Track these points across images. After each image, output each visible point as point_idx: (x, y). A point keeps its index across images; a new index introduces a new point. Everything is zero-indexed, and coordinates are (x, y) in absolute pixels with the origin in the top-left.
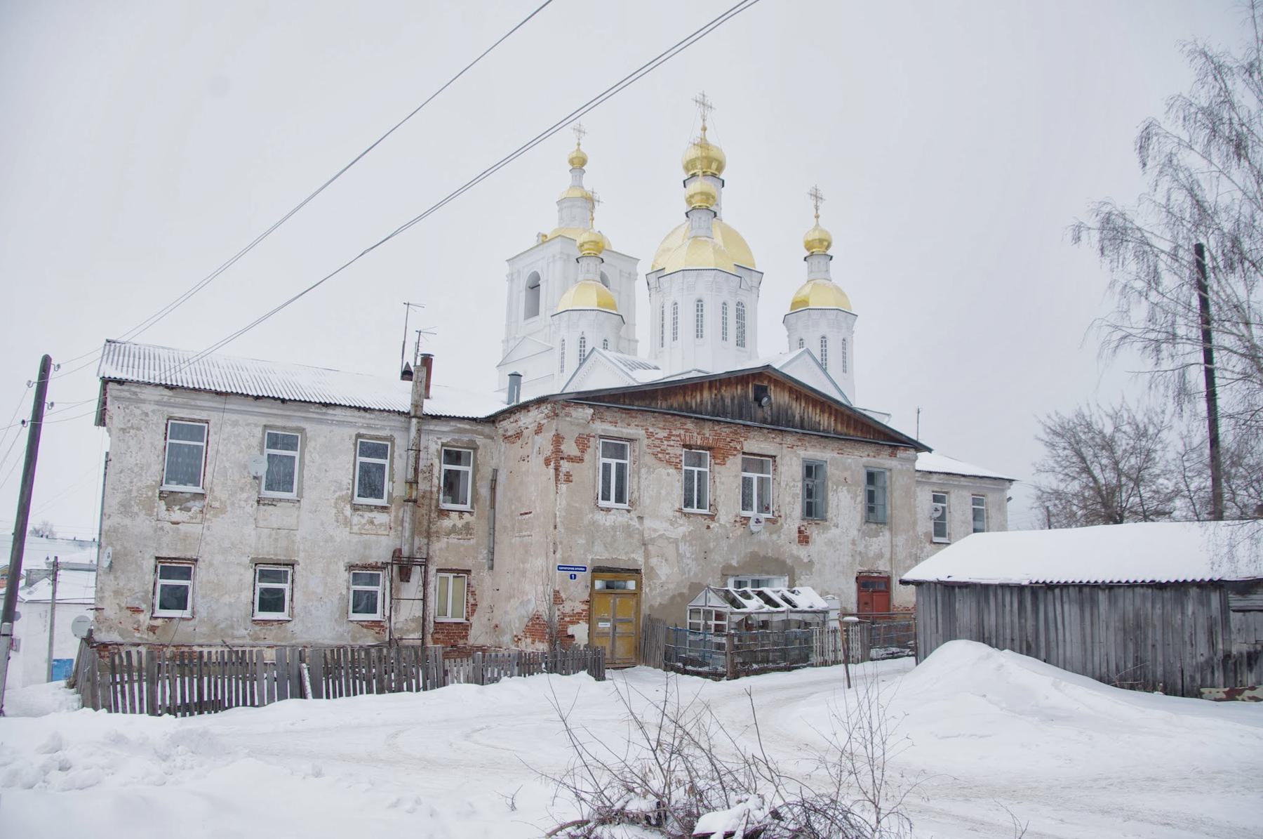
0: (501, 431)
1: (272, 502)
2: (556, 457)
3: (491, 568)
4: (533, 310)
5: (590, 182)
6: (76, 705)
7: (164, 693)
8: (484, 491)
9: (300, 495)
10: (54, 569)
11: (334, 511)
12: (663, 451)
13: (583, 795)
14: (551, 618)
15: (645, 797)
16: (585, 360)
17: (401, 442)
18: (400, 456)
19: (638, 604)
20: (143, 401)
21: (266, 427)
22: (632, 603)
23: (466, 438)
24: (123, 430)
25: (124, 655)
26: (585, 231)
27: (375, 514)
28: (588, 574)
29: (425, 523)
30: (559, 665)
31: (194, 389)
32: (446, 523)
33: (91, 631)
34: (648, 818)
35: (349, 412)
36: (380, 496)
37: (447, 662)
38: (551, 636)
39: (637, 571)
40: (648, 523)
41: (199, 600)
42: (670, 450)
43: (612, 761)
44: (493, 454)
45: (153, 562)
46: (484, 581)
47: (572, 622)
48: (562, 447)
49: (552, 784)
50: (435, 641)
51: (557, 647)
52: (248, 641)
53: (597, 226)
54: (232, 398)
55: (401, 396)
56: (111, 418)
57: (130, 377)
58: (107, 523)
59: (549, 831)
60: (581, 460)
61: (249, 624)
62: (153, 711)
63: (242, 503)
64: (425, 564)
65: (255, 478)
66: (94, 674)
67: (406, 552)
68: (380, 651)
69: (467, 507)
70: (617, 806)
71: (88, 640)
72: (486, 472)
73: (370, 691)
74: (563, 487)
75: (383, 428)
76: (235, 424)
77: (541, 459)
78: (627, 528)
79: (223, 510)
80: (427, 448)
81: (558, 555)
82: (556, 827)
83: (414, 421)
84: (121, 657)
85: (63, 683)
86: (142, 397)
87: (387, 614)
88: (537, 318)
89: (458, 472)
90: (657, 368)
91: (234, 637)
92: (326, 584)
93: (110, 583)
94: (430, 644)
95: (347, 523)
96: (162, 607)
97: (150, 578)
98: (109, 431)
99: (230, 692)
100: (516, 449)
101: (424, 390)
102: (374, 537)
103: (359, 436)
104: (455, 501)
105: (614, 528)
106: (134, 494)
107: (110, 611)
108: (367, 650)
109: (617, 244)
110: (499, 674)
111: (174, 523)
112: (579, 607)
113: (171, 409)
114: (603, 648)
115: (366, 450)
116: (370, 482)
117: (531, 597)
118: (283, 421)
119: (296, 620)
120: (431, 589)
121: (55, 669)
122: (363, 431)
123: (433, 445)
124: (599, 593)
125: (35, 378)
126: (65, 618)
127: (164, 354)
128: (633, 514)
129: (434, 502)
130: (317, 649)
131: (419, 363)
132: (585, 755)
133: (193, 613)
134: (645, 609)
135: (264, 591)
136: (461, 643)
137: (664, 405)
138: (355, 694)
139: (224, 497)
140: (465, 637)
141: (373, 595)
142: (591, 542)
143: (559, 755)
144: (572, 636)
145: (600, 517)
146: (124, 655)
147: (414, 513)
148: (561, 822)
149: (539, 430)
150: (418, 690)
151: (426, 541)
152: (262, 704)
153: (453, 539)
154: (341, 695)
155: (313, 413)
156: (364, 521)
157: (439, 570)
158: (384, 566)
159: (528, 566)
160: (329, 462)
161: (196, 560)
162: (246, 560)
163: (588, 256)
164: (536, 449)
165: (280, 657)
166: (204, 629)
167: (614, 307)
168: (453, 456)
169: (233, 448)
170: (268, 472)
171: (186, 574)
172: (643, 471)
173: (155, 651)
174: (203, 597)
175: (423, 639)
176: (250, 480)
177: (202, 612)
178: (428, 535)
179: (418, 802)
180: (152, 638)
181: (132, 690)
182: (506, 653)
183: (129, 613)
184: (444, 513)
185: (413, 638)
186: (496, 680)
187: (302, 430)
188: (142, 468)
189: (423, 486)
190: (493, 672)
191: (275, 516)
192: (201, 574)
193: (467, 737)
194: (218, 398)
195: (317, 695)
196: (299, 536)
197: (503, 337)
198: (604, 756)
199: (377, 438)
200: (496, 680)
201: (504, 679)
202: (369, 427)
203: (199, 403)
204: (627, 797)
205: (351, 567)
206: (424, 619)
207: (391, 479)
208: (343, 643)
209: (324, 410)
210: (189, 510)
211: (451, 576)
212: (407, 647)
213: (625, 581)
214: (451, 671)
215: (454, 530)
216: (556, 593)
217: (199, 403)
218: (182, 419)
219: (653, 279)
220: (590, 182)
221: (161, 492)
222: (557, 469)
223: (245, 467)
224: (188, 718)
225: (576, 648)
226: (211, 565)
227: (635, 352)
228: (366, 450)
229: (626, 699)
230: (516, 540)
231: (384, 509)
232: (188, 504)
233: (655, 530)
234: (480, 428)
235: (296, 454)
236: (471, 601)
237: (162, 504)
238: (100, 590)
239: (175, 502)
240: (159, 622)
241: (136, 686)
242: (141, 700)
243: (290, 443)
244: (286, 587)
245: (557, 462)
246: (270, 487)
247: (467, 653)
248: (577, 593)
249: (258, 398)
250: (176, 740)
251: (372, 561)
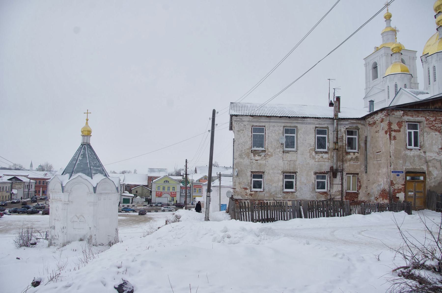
0: (367, 122)
1: (288, 152)
2: (390, 130)
3: (366, 172)
4: (375, 76)
5: (393, 24)
6: (229, 218)
7: (256, 215)
8: (362, 145)
9: (297, 149)
10: (220, 176)
11: (309, 154)
12: (433, 126)
13: (407, 257)
14: (390, 190)
15: (433, 260)
16: (397, 93)
17: (331, 128)
18: (331, 134)
19: (425, 186)
20: (244, 121)
21: (284, 126)
22: (423, 185)
23: (354, 126)
24: (238, 131)
25: (243, 203)
26: (393, 43)
27: (323, 154)
28: (404, 174)
29: (341, 157)
30: (393, 208)
31: (260, 116)
32: (349, 157)
33: (232, 195)
34: (434, 268)
35: (312, 120)
36: (324, 148)
37: (351, 206)
38: (390, 197)
39: (424, 173)
40: (428, 154)
41: (265, 185)
42: (436, 125)
43: (418, 245)
44: (366, 131)
45: (250, 173)
46: (364, 177)
47: (398, 192)
48: (392, 127)
49: (395, 252)
50: (346, 199)
51: (392, 201)
52: (282, 199)
53: (398, 40)
54: (272, 118)
55: (330, 112)
56: (234, 127)
57: (239, 114)
58: (235, 161)
59: (394, 269)
60: (400, 131)
61: (282, 193)
62: (253, 221)
63: (278, 153)
64: (342, 171)
65: (282, 144)
66: (234, 209)
67: (335, 167)
68: (327, 202)
69: (356, 151)
70: (421, 262)
71: (232, 198)
72: (363, 137)
73: (324, 216)
74: (393, 142)
75: (324, 124)
76: (274, 126)
77: (384, 131)
78: (419, 156)
79: (271, 155)
80: (340, 130)
81: (392, 167)
82: (396, 268)
83: (335, 121)
84: (242, 204)
85: (225, 211)
86: (243, 120)
87: (329, 189)
88: (377, 79)
89: (352, 138)
90: (427, 93)
91: (277, 197)
93: (238, 181)
94: (344, 200)
95: (314, 158)
96: (254, 187)
97: (249, 178)
98: (234, 132)
99: (277, 216)
100: (374, 129)
101: (338, 110)
102: (324, 163)
103: (316, 127)
104: (352, 149)
105: (414, 156)
106: (243, 151)
107: (238, 189)
108: (323, 202)
109: (407, 46)
110: (370, 211)
111: (256, 160)
112: (401, 187)
113: (253, 123)
114: (411, 202)
115: (319, 132)
116: (321, 143)
117: (382, 183)
118: (290, 124)
119: (297, 192)
120: (344, 181)
121: (222, 207)
122: (317, 126)
123: (342, 129)
124: (409, 181)
125: (211, 117)
126: (224, 192)
127: (249, 105)
128: (421, 151)
129: (344, 149)
130: (306, 202)
131: (335, 100)
132: (407, 242)
133: (264, 190)
134: (427, 187)
135: (287, 182)
136: (356, 200)
137: (433, 107)
138: (319, 217)
139: (272, 151)
140: (357, 197)
141: (323, 183)
142: (405, 162)
143: (399, 242)
144: (398, 198)
145: (408, 152)
146: (243, 203)
147: (337, 154)
148: (399, 267)
149: (382, 121)
150: (341, 216)
151: (342, 163)
152: (287, 220)
153: (352, 163)
154: (314, 217)
155: (300, 121)
156: (319, 157)
157: (347, 174)
158: (327, 173)
159: (380, 171)
160: (306, 137)
161: (264, 172)
162: (280, 172)
163: (396, 53)
164: (381, 128)
165: (293, 204)
166: (267, 195)
167: (408, 71)
168: (350, 132)
169: (274, 135)
170: (286, 142)
171: (261, 177)
172: (425, 134)
173: (252, 202)
174: (267, 184)
175: (342, 198)
176: (280, 145)
177: (267, 189)
178: (343, 161)
179: (344, 255)
180: (251, 198)
181: (246, 214)
182: (373, 204)
183: (244, 189)
184: (348, 153)
185: (338, 198)
186: (369, 213)
187: (296, 127)
188: (245, 143)
189: (340, 144)
190: (368, 210)
191: (289, 157)
192: (266, 176)
193: (359, 233)
194: (268, 118)
195: (306, 217)
196: (298, 162)
197: (365, 88)
198: (415, 243)
199: (322, 128)
200: (370, 213)
201: (372, 213)
202: (319, 124)
203: (261, 120)
204: (425, 259)
205: (315, 173)
206: (342, 191)
207: (328, 142)
208: (314, 199)
209: (303, 119)
210: (261, 156)
211: (351, 176)
212: (337, 201)
213: (419, 177)
214: (353, 210)
215: (352, 159)
216: (392, 181)
217: (261, 120)
218: (256, 126)
219: (423, 58)
220: (393, 24)
221: (252, 150)
222: (390, 135)
223: (278, 141)
224: (264, 224)
225: (400, 202)
226: (269, 173)
227: (417, 88)
228: (319, 132)
229: (424, 222)
230: (375, 162)
231: (326, 153)
232: (260, 154)
233: (431, 157)
234: (359, 122)
235: (295, 135)
236: (359, 185)
237: (252, 155)
238: (234, 182)
239: (256, 153)
240: (253, 193)
241: (247, 213)
242: (249, 217)
243: (292, 131)
244: (294, 180)
245: (390, 132)
246: (286, 147)
247: (358, 203)
248: (399, 182)
249: (281, 117)
250: (262, 230)
251: (323, 171)
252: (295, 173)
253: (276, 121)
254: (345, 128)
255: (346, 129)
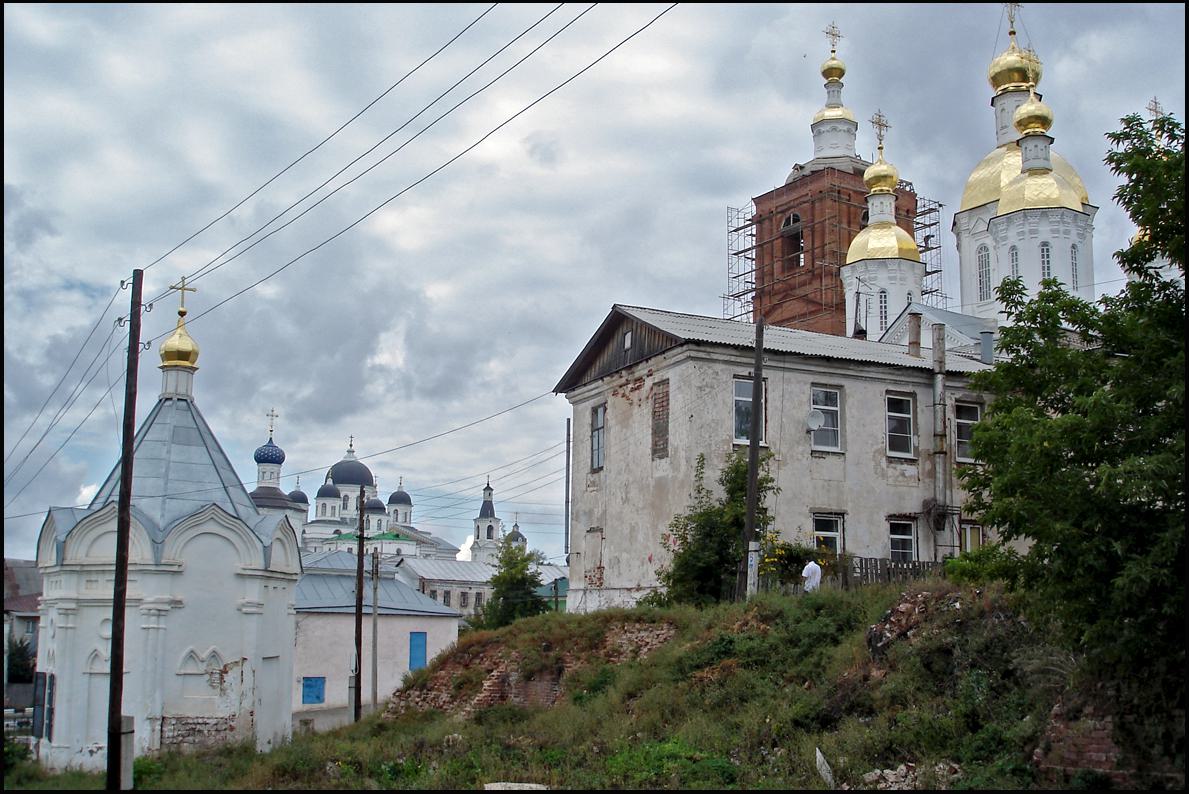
11: (873, 463)
18: (922, 411)
24: (700, 388)
27: (905, 466)
54: (787, 358)
63: (800, 457)
83: (940, 377)
92: (871, 533)
95: (884, 475)
103: (888, 392)
116: (898, 440)
162: (806, 510)
202: (896, 382)
203: (715, 357)
217: (787, 365)
252: (842, 514)
253: (826, 370)
254: (953, 397)
255: (957, 401)
